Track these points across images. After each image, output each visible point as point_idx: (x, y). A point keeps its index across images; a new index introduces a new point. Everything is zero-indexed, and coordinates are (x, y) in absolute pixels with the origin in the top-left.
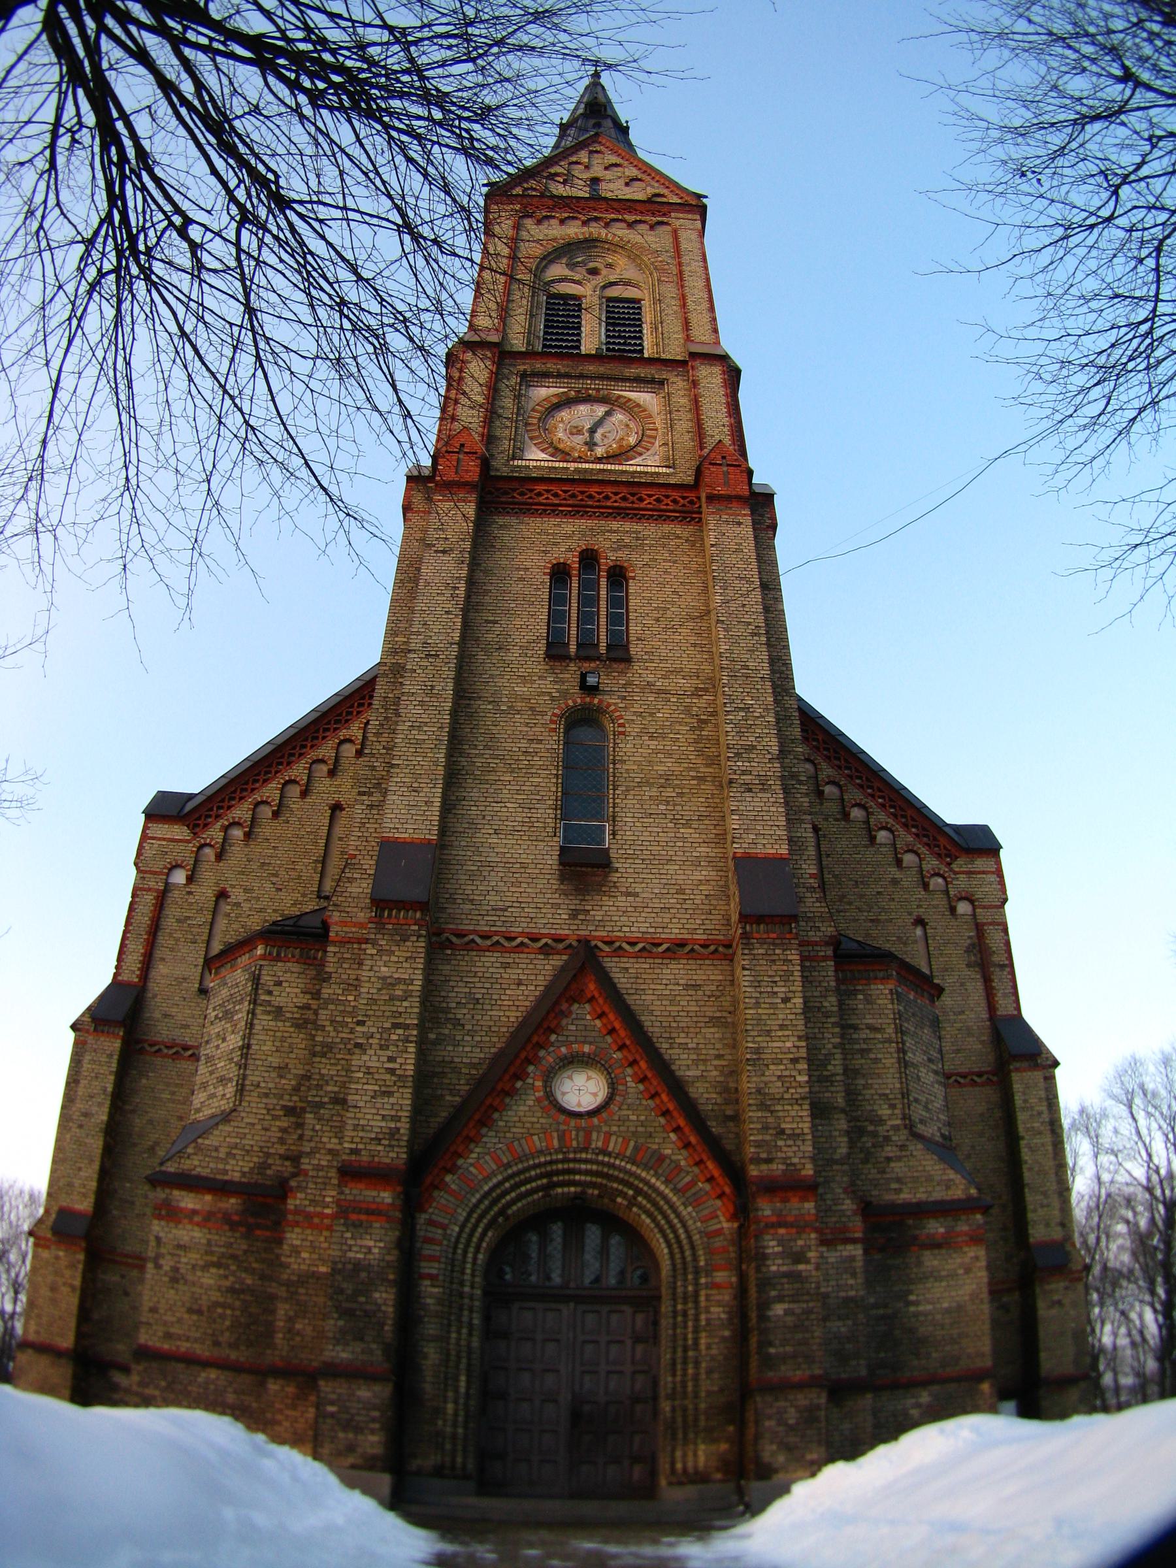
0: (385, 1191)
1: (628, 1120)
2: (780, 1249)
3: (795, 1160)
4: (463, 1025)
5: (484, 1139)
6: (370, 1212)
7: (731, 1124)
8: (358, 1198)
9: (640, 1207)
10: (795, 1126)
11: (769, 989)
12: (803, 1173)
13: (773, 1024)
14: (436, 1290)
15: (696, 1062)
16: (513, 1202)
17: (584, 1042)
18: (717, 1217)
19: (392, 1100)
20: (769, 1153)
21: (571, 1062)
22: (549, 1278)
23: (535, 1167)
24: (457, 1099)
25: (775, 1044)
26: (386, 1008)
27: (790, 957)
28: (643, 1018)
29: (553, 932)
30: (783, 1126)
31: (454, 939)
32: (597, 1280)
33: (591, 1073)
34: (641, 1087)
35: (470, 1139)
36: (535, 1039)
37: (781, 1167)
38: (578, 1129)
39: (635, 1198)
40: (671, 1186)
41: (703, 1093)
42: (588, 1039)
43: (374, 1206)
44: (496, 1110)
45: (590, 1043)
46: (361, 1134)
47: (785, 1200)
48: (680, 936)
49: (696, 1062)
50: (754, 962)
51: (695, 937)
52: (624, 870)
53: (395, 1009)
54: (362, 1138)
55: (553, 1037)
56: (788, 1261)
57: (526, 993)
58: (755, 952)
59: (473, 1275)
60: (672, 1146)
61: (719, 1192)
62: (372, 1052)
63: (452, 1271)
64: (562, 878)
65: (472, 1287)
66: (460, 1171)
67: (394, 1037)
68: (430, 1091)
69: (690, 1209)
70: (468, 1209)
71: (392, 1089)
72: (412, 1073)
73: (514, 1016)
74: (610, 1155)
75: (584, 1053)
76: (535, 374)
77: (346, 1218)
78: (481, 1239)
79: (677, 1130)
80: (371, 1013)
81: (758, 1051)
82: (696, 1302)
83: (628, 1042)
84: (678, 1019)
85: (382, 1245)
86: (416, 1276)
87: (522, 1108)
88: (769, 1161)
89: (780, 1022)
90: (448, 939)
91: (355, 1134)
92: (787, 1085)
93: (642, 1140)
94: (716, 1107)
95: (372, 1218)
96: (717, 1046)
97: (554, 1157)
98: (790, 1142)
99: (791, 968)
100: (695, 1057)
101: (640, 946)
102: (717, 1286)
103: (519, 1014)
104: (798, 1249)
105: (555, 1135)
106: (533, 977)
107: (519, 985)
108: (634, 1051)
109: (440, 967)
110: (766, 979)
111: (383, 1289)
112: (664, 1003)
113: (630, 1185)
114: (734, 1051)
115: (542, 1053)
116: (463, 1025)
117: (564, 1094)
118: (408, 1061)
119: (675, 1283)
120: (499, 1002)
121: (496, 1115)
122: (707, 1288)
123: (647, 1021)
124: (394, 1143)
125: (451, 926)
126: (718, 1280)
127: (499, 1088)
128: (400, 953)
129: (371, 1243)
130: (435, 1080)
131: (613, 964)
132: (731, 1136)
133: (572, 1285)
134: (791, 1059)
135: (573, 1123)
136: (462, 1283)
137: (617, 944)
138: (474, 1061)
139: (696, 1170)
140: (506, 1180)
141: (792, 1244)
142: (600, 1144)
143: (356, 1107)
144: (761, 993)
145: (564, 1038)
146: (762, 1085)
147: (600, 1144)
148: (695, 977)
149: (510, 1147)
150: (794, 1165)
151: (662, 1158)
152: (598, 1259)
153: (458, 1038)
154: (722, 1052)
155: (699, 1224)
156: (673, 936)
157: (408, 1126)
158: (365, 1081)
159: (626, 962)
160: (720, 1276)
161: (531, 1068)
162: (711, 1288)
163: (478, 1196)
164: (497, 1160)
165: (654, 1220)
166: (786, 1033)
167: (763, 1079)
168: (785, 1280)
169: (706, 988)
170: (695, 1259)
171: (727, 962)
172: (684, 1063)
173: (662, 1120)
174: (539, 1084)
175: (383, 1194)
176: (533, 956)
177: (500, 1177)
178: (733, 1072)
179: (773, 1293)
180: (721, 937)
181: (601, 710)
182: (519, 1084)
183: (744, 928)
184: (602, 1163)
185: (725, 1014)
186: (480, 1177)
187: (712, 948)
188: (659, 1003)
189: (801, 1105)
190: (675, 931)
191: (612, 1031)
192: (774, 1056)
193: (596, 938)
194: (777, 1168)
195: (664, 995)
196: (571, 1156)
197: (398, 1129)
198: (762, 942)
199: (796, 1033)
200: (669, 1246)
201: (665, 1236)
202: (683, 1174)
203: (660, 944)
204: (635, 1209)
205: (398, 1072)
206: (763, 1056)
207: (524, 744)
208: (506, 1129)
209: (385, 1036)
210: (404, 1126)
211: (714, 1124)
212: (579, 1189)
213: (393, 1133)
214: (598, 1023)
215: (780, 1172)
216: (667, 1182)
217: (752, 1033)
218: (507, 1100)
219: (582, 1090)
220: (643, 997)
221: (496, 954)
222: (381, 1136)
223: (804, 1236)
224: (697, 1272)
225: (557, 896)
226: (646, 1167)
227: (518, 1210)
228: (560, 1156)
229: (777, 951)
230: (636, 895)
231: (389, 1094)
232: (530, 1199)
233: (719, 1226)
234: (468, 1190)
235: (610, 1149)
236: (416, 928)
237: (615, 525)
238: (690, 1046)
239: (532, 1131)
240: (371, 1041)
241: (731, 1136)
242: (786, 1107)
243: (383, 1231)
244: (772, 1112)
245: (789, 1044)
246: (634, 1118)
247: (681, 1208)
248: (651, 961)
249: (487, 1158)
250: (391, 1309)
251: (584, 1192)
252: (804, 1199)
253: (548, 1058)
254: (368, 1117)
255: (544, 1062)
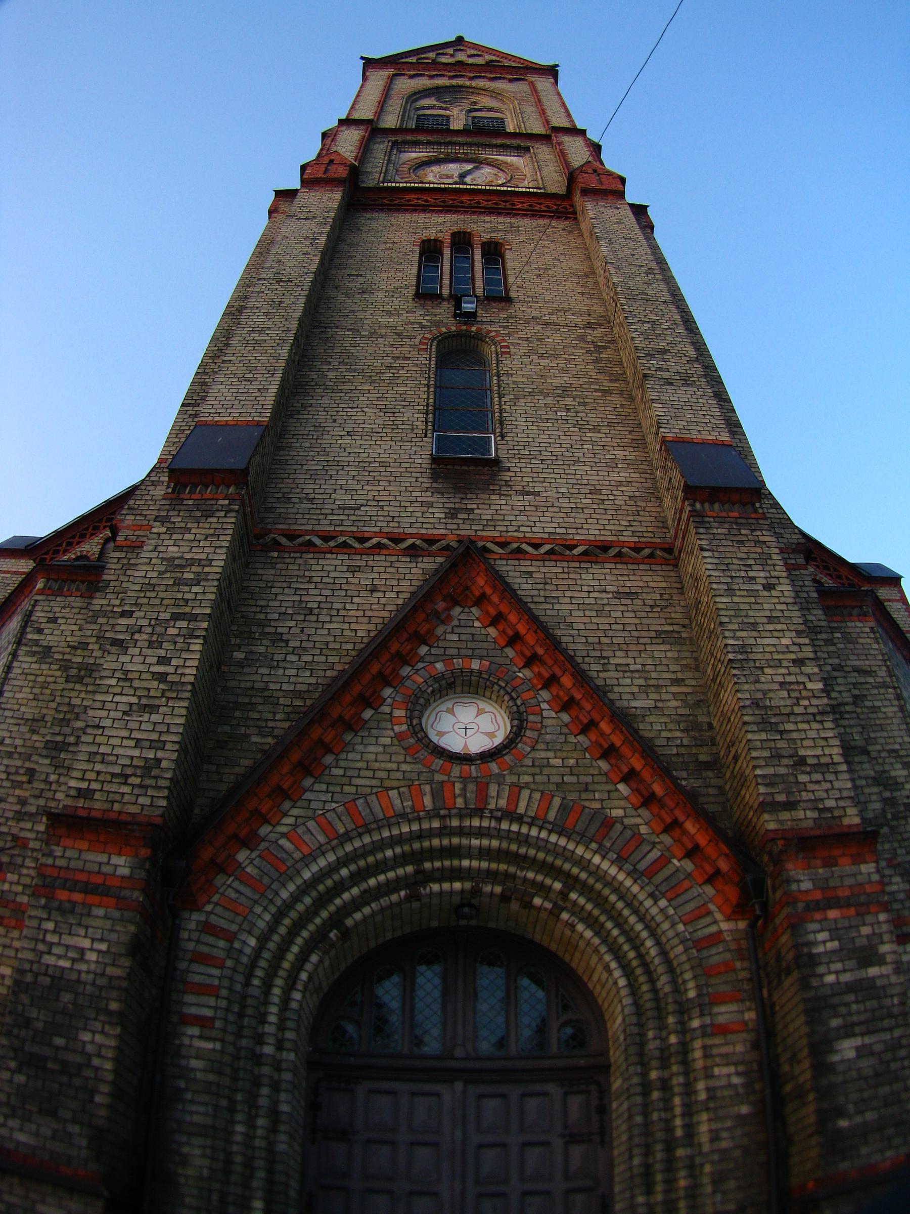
0: (120, 854)
1: (549, 765)
2: (835, 944)
3: (831, 803)
4: (287, 642)
5: (308, 795)
6: (89, 889)
7: (710, 774)
8: (73, 864)
9: (576, 910)
10: (819, 752)
11: (743, 574)
12: (846, 821)
13: (759, 616)
14: (209, 1045)
15: (645, 689)
16: (356, 905)
17: (471, 657)
18: (709, 913)
19: (155, 718)
20: (789, 793)
21: (451, 686)
22: (419, 1042)
23: (394, 841)
24: (270, 740)
25: (766, 641)
26: (168, 595)
27: (761, 539)
28: (559, 632)
29: (423, 531)
30: (802, 752)
31: (283, 541)
32: (501, 1043)
33: (483, 705)
34: (565, 717)
35: (283, 794)
36: (394, 647)
37: (809, 814)
38: (465, 779)
39: (564, 895)
40: (628, 867)
41: (661, 729)
42: (477, 652)
43: (99, 880)
44: (329, 750)
45: (481, 658)
46: (98, 767)
47: (830, 863)
48: (602, 538)
49: (645, 689)
50: (715, 542)
51: (621, 539)
52: (519, 471)
53: (179, 595)
54: (98, 773)
55: (423, 650)
56: (850, 964)
57: (383, 601)
58: (715, 531)
59: (282, 1027)
60: (623, 803)
61: (710, 870)
62: (137, 651)
63: (241, 1015)
64: (435, 476)
65: (279, 1046)
66: (263, 845)
67: (172, 631)
68: (227, 729)
69: (663, 903)
70: (273, 909)
71: (157, 702)
72: (191, 679)
73: (363, 630)
74: (520, 819)
75: (472, 671)
76: (405, 142)
77: (51, 897)
78: (298, 966)
79: (629, 777)
80: (145, 601)
81: (743, 649)
82: (686, 1063)
83: (540, 651)
84: (611, 633)
85: (103, 947)
86: (175, 1018)
87: (372, 749)
88: (790, 806)
89: (768, 614)
90: (274, 539)
91: (90, 766)
92: (796, 694)
93: (573, 796)
94: (682, 751)
95: (91, 899)
96: (672, 668)
97: (426, 825)
98: (817, 777)
99: (766, 550)
100: (642, 682)
101: (547, 547)
102: (722, 1030)
103: (372, 627)
104: (864, 941)
105: (427, 788)
106: (395, 582)
107: (372, 591)
108: (550, 662)
109: (260, 572)
110: (735, 561)
111: (98, 1026)
112: (588, 613)
113: (556, 872)
114: (697, 675)
115: (405, 671)
116: (287, 642)
117: (441, 734)
118: (192, 647)
119: (642, 1035)
120: (342, 613)
121: (328, 759)
122: (704, 1035)
123: (564, 636)
124: (148, 782)
125: (281, 527)
126: (721, 1019)
127: (335, 713)
128: (197, 531)
129: (87, 943)
130: (238, 714)
131: (509, 568)
132: (712, 791)
133: (459, 1052)
134: (794, 661)
135: (456, 770)
136: (260, 1039)
137: (515, 545)
138: (299, 687)
139: (667, 839)
140: (343, 862)
141: (853, 934)
142: (503, 803)
143: (98, 727)
144: (732, 577)
145: (441, 651)
146: (759, 695)
147: (503, 803)
148: (628, 584)
149: (350, 807)
150: (830, 810)
151: (608, 823)
152: (501, 1012)
153: (276, 657)
154: (680, 675)
155: (681, 927)
156: (592, 538)
157: (175, 756)
158: (118, 690)
159: (526, 566)
160: (725, 1013)
161: (387, 692)
162: (713, 1035)
163: (292, 887)
164: (327, 828)
165: (599, 929)
166: (779, 627)
167: (758, 686)
168: (851, 997)
169: (644, 596)
170: (677, 988)
171: (671, 568)
172: (627, 689)
173: (604, 765)
174: (399, 713)
175: (117, 860)
176: (394, 558)
177: (331, 857)
178: (704, 698)
179: (835, 1022)
180: (658, 540)
181: (479, 337)
182: (368, 714)
183: (693, 505)
184: (508, 836)
185: (676, 628)
186: (297, 855)
187: (647, 551)
188: (581, 613)
189: (821, 722)
190: (593, 532)
191: (514, 640)
192: (768, 656)
193: (483, 538)
194: (805, 816)
195: (584, 606)
196: (455, 823)
197: (158, 761)
198: (722, 522)
199: (792, 627)
200: (628, 972)
201: (619, 957)
202: (645, 848)
203: (575, 546)
204: (565, 916)
205: (170, 678)
206: (751, 656)
207: (388, 361)
208: (345, 780)
209: (159, 629)
210: (168, 757)
211: (684, 774)
212: (468, 885)
213: (150, 767)
214: (492, 631)
215: (810, 823)
216: (620, 861)
217: (730, 627)
218: (348, 737)
219: (470, 727)
220: (557, 607)
221: (340, 556)
222: (129, 771)
223: (869, 919)
224: (683, 1010)
225: (429, 494)
226: (583, 838)
227: (365, 919)
228: (436, 824)
229: (743, 532)
230: (537, 494)
231: (152, 709)
232: (384, 901)
233: (713, 929)
234: (275, 875)
235: (521, 810)
236: (227, 502)
237: (488, 219)
238: (632, 668)
239: (387, 783)
240: (137, 636)
241: (712, 791)
242: (801, 726)
243: (108, 924)
244: (781, 733)
245: (785, 641)
246: (558, 762)
247: (648, 903)
248: (565, 564)
249: (311, 824)
250: (108, 1066)
251: (476, 892)
252: (858, 860)
253: (415, 677)
254: (113, 741)
255: (408, 683)
